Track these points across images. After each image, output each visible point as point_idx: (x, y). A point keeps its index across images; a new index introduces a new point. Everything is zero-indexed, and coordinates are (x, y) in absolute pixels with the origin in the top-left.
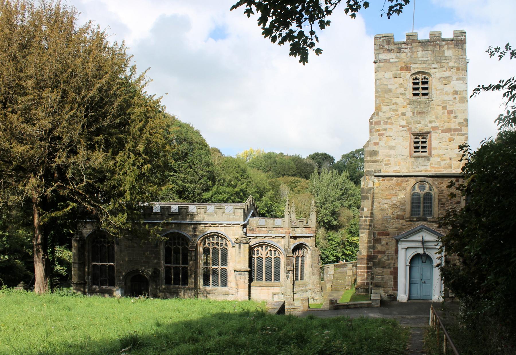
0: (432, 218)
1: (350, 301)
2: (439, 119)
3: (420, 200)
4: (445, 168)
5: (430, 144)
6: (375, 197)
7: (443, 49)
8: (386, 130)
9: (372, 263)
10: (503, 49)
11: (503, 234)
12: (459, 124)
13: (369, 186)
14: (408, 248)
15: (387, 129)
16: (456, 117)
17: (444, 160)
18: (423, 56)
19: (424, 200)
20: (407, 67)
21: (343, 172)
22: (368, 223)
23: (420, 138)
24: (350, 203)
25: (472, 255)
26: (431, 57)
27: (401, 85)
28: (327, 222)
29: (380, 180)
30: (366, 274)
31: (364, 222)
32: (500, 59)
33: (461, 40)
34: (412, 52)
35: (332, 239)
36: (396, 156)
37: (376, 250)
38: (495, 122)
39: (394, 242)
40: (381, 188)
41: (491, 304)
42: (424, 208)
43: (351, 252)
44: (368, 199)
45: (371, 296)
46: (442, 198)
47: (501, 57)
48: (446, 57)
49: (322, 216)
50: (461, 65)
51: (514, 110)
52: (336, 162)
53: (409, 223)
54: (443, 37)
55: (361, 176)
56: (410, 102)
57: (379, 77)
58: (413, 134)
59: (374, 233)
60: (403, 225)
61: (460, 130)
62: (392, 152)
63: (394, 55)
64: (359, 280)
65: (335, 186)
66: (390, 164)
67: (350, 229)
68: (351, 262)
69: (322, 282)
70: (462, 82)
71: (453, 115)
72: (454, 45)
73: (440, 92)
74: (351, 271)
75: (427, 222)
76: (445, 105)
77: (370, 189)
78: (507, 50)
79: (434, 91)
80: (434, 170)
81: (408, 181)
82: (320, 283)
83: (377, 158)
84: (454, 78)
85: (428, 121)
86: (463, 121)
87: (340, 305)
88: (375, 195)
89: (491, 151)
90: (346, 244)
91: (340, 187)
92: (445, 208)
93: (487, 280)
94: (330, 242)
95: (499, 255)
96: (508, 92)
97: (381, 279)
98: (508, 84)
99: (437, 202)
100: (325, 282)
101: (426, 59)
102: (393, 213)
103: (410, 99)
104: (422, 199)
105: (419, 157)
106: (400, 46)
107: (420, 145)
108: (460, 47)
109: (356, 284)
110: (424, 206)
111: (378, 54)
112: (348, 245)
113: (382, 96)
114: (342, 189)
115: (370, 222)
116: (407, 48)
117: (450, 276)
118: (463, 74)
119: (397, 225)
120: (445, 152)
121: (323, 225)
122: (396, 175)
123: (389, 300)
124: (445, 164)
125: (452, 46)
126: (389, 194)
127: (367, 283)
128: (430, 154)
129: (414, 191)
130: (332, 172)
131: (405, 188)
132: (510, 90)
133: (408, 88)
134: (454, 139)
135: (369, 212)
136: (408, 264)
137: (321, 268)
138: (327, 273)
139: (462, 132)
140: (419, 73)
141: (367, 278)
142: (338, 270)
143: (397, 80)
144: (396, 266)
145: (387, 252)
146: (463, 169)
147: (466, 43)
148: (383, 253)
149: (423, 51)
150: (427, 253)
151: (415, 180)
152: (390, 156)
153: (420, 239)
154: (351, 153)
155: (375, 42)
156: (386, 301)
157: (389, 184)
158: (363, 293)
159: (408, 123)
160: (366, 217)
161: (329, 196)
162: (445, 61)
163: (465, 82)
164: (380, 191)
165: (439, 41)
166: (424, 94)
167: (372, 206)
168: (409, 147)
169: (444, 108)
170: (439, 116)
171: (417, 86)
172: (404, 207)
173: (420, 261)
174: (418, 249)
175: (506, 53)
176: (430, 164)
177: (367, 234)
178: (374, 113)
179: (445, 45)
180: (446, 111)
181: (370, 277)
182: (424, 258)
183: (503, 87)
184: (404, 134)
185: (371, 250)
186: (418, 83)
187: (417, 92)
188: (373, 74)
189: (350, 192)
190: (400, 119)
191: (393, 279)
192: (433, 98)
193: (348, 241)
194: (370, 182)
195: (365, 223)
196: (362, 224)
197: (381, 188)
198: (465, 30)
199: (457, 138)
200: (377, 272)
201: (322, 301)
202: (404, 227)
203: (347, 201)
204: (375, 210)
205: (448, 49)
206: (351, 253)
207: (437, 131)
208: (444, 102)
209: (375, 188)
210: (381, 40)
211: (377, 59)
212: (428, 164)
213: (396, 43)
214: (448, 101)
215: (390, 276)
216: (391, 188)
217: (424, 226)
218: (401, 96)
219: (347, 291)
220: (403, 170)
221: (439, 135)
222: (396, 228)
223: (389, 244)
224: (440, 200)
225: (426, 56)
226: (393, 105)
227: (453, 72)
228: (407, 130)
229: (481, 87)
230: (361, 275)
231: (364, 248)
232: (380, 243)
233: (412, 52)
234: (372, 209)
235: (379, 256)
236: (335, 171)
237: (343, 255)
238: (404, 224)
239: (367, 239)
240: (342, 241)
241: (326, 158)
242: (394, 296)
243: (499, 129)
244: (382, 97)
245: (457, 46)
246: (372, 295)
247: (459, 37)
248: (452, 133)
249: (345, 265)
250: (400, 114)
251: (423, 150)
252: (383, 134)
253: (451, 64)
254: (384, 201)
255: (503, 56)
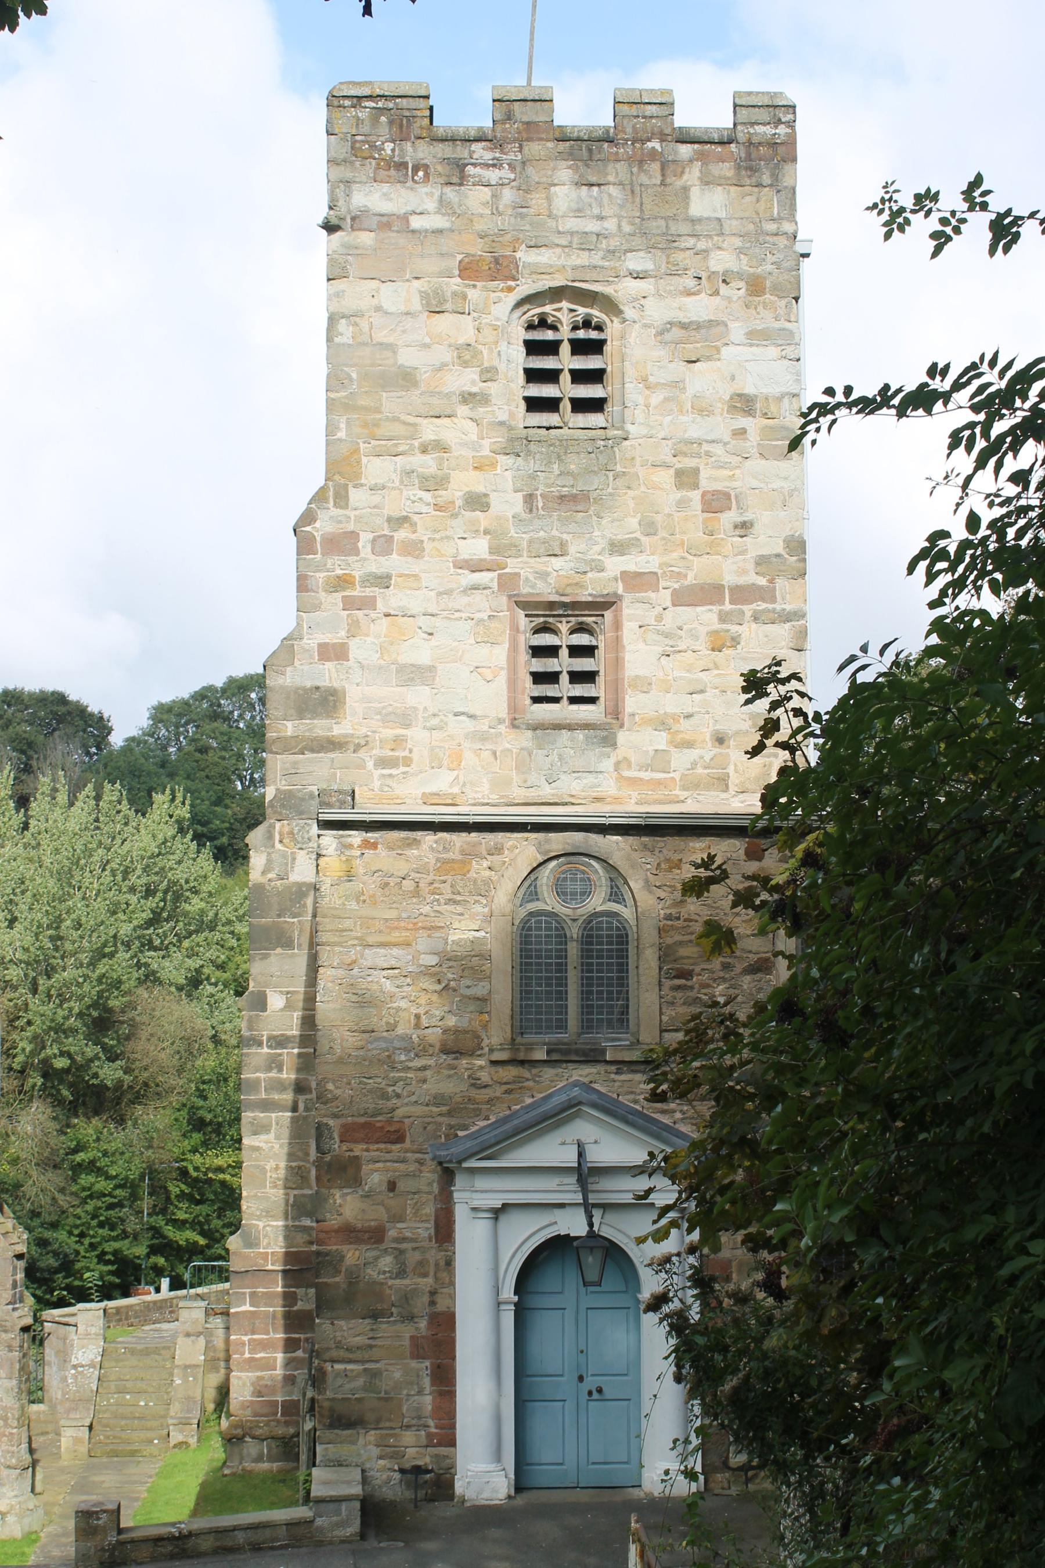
0: (631, 1047)
1: (195, 1513)
2: (663, 533)
3: (563, 954)
4: (692, 785)
5: (618, 663)
6: (323, 937)
7: (679, 183)
8: (383, 581)
9: (312, 1291)
10: (951, 201)
11: (961, 1135)
12: (762, 562)
13: (295, 877)
14: (505, 1207)
15: (389, 577)
16: (744, 527)
17: (689, 744)
18: (579, 212)
19: (586, 953)
20: (496, 261)
21: (158, 798)
22: (288, 1075)
23: (564, 628)
24: (194, 963)
25: (809, 1249)
26: (620, 218)
27: (465, 355)
28: (67, 1071)
29: (350, 846)
30: (280, 1357)
31: (269, 1069)
32: (937, 251)
33: (773, 144)
34: (525, 188)
35: (92, 1162)
36: (435, 722)
37: (333, 1221)
38: (911, 568)
39: (430, 1176)
40: (357, 886)
41: (919, 1504)
42: (586, 995)
43: (203, 1233)
44: (288, 944)
45: (308, 1481)
46: (681, 943)
47: (941, 240)
48: (694, 221)
49: (35, 1037)
50: (769, 267)
51: (998, 512)
52: (117, 740)
53: (509, 1073)
54: (681, 120)
55: (254, 817)
56: (511, 440)
57: (350, 304)
58: (527, 606)
59: (321, 1131)
60: (476, 1085)
61: (767, 594)
62: (418, 697)
63: (432, 194)
64: (241, 1393)
65: (113, 872)
66: (407, 762)
67: (194, 1108)
68: (199, 1290)
69: (35, 1407)
70: (773, 351)
71: (731, 517)
72: (738, 168)
73: (667, 399)
74: (202, 1341)
75: (601, 1068)
76: (689, 463)
77: (302, 891)
78: (971, 209)
79: (634, 393)
80: (635, 795)
81: (498, 850)
82: (26, 1422)
83: (338, 730)
84: (737, 330)
85: (603, 544)
86: (779, 548)
87: (132, 1541)
88: (323, 922)
89: (899, 711)
90: (174, 1188)
91: (138, 879)
92: (692, 994)
93: (891, 1377)
94: (86, 1180)
95: (944, 1244)
96: (971, 425)
97: (360, 1382)
98: (968, 382)
99: (654, 964)
100: (53, 1407)
101: (593, 226)
102: (425, 1022)
103: (511, 428)
104: (573, 950)
105: (558, 727)
106: (461, 152)
107: (564, 663)
108: (766, 179)
109: (229, 1415)
110: (587, 983)
111: (348, 183)
112: (182, 1196)
113: (362, 402)
114: (149, 892)
115: (299, 1070)
116: (496, 165)
117: (718, 1357)
118: (781, 311)
119: (449, 1087)
120: (690, 704)
121: (44, 1086)
122: (437, 819)
123: (409, 1494)
124: (694, 765)
125: (726, 169)
126: (399, 919)
127: (290, 1408)
128: (616, 712)
129: (533, 906)
130: (98, 798)
131: (484, 890)
132: (981, 417)
133: (502, 367)
134: (735, 641)
135: (297, 1015)
136: (508, 1293)
137: (25, 1329)
138: (64, 1356)
139: (778, 607)
140: (556, 294)
141: (289, 1380)
142: (126, 1337)
143: (443, 323)
144: (441, 1306)
145: (392, 1233)
146: (769, 797)
147: (794, 160)
148: (375, 1235)
149: (578, 184)
150: (606, 1232)
151: (539, 847)
152: (405, 719)
153: (569, 1157)
154: (202, 695)
155: (329, 122)
156: (393, 1504)
157: (401, 867)
158: (265, 1466)
159: (502, 548)
160: (280, 1042)
161: (78, 925)
162: (691, 242)
163: (790, 351)
164: (353, 905)
165: (663, 138)
166: (581, 406)
167: (312, 980)
168: (503, 676)
169: (686, 478)
170: (659, 518)
171: (547, 363)
172: (480, 990)
173: (572, 1279)
174: (558, 1212)
175: (964, 221)
176: (617, 766)
177: (286, 1133)
178: (323, 490)
179: (691, 161)
180: (696, 495)
181: (302, 1374)
182: (591, 1261)
183: (946, 397)
184: (482, 604)
185: (307, 1222)
186: (551, 348)
187: (547, 391)
188: (320, 287)
189: (195, 905)
190: (457, 526)
191: (427, 1382)
192: (629, 427)
193: (184, 1173)
194: (301, 856)
195: (273, 1074)
196: (258, 1081)
197: (357, 886)
198: (792, 95)
199: (748, 631)
200: (339, 1346)
201: (33, 1522)
202: (483, 1095)
203: (178, 956)
204: (327, 1007)
205: (707, 181)
206: (202, 1241)
207: (652, 595)
208: (685, 447)
209: (325, 888)
210: (363, 114)
211: (343, 211)
212: (608, 764)
213: (441, 132)
214: (706, 447)
215: (414, 1364)
216: (408, 885)
217: (587, 1087)
218: (463, 410)
219: (180, 1455)
220: (471, 795)
221: (659, 618)
222: (438, 1100)
223: (401, 1186)
224: (666, 954)
225: (596, 211)
226: (424, 451)
227: (729, 299)
228: (495, 585)
229: (840, 397)
230: (252, 1364)
231: (269, 1214)
232: (356, 1181)
233: (525, 188)
234: (310, 1000)
235: (352, 1255)
236: (112, 792)
237: (153, 1250)
238: (484, 1076)
239: (283, 1164)
240: (151, 1171)
241: (60, 719)
242: (439, 1476)
243: (933, 605)
244: (366, 409)
245: (753, 170)
246: (315, 1471)
247: (760, 129)
248: (728, 606)
249: (167, 1311)
250: (459, 503)
251: (579, 690)
252: (369, 603)
253: (721, 260)
254: (381, 957)
255: (949, 239)
